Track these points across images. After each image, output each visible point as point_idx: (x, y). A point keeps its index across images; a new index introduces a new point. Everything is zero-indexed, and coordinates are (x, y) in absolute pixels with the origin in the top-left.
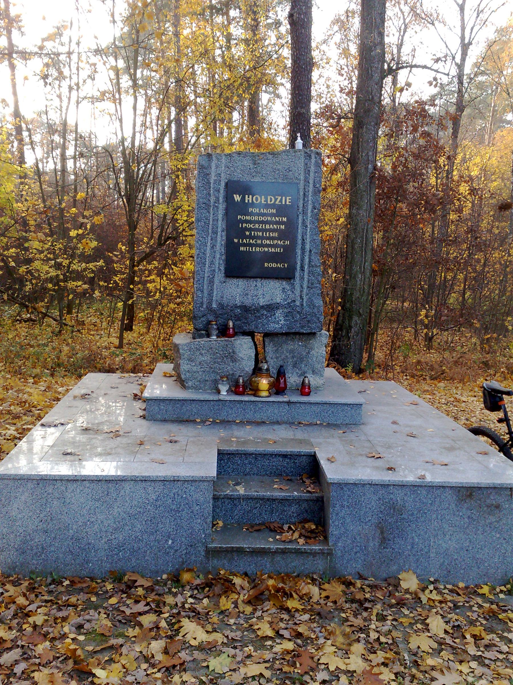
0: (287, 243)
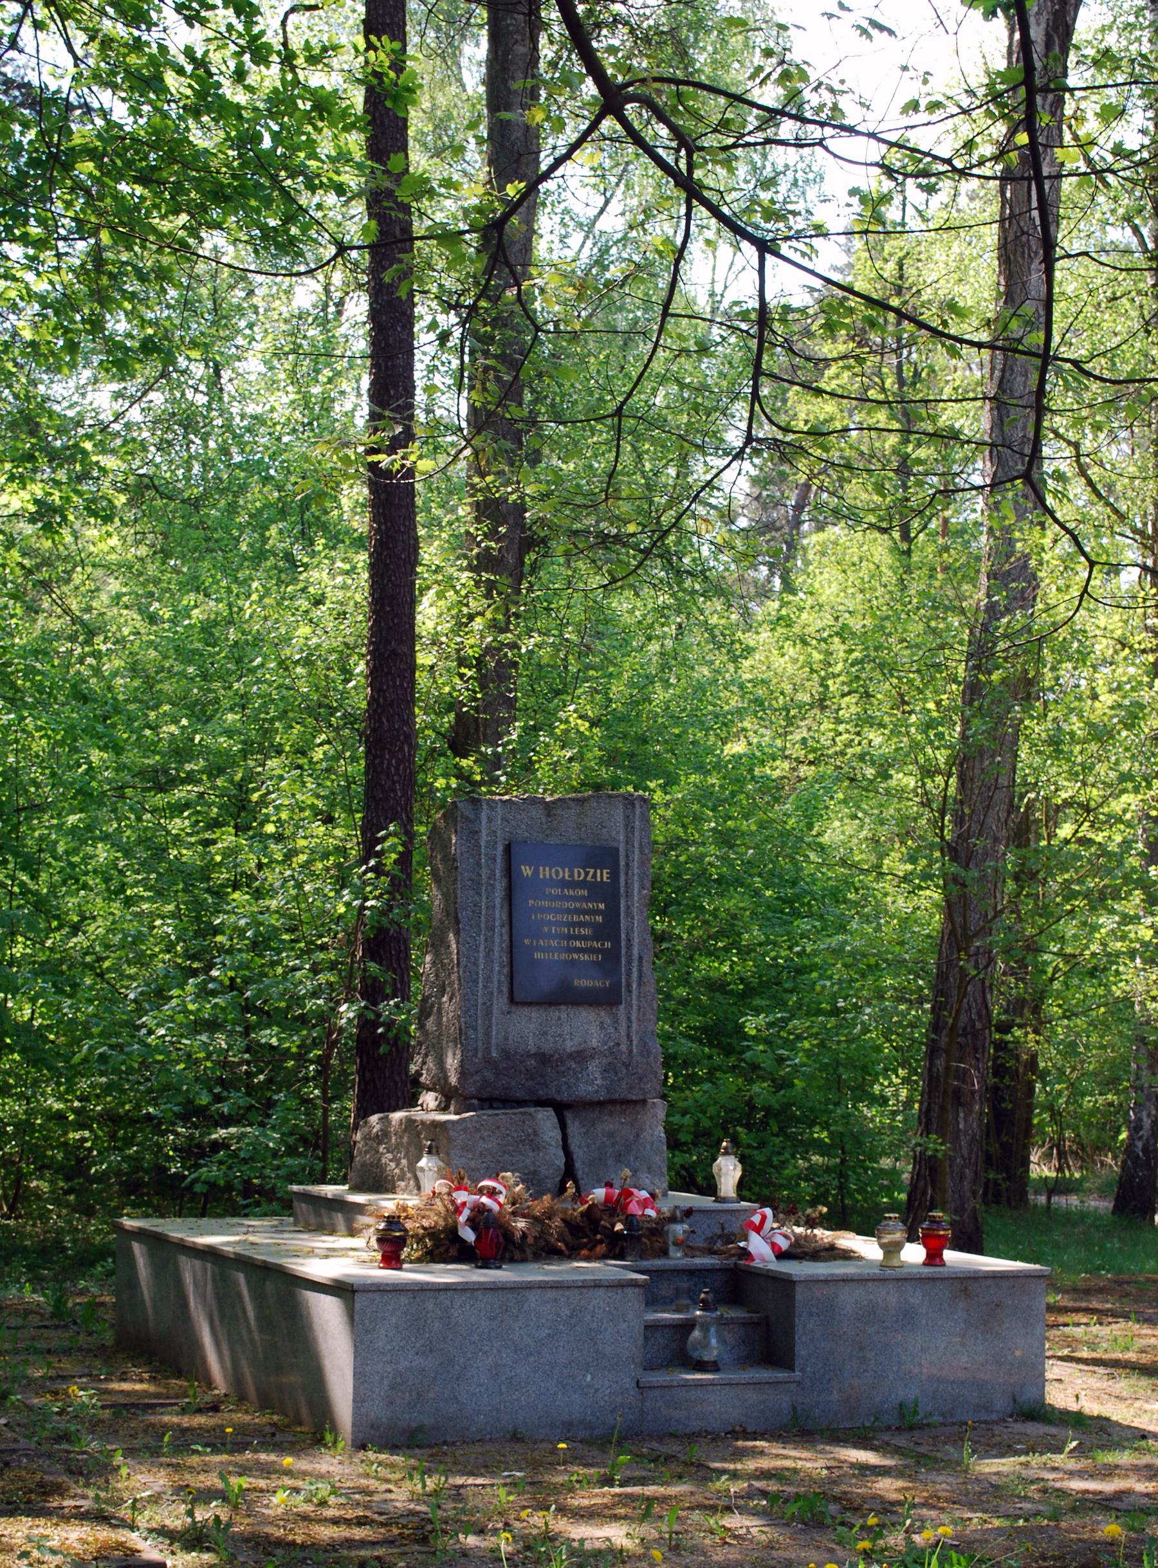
0: (608, 945)
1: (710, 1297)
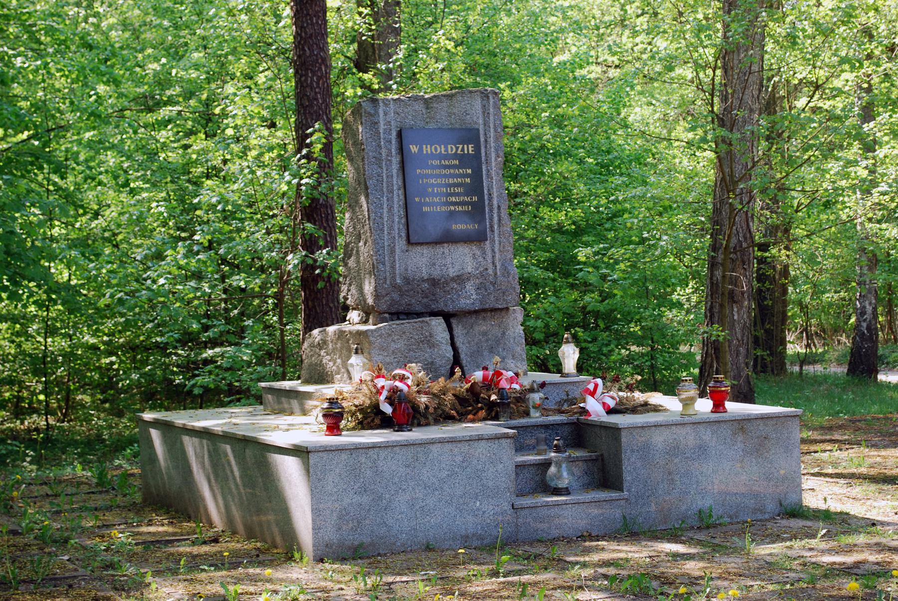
0: (475, 199)
1: (561, 442)
